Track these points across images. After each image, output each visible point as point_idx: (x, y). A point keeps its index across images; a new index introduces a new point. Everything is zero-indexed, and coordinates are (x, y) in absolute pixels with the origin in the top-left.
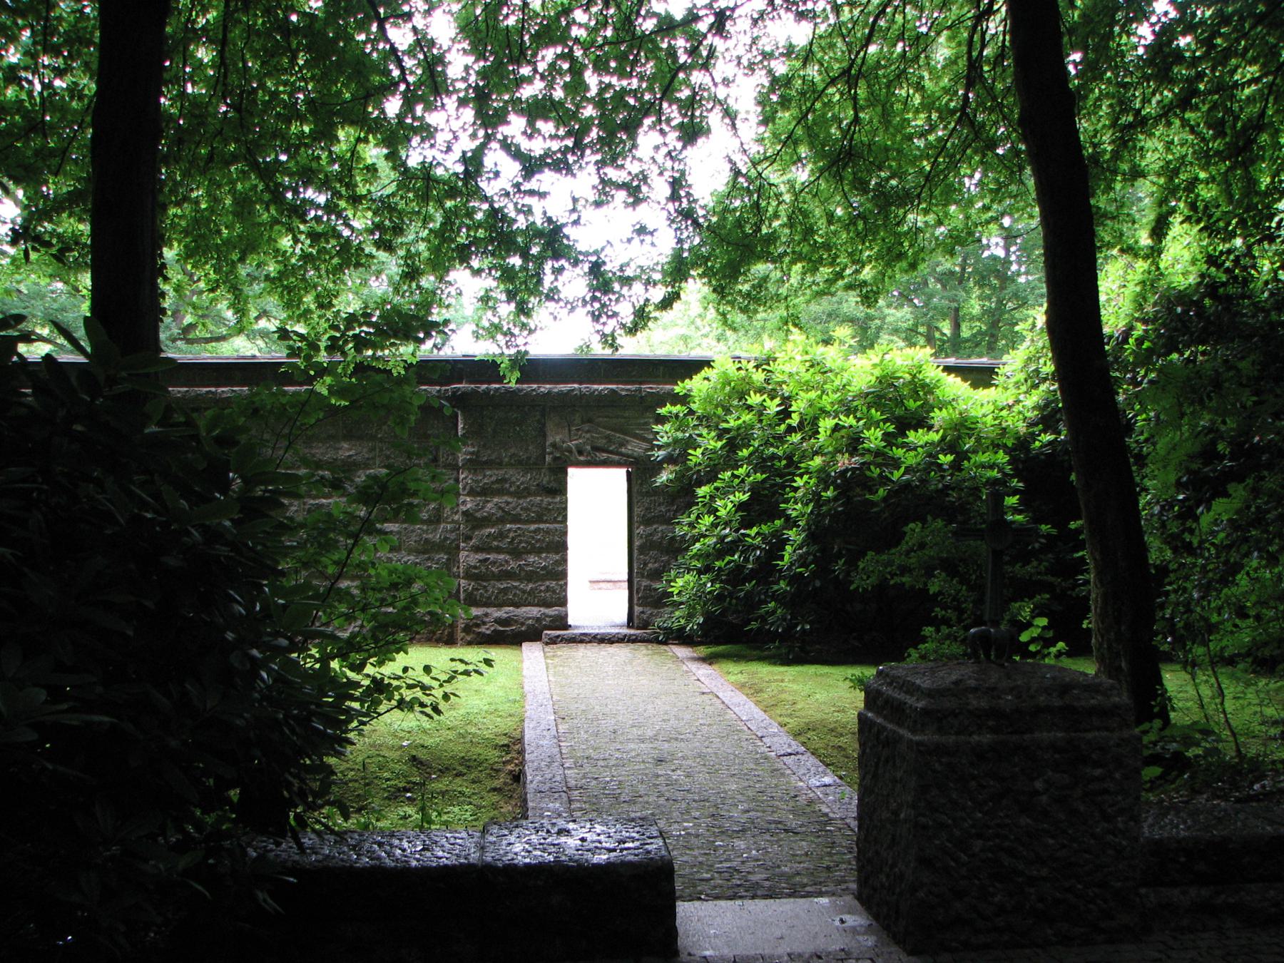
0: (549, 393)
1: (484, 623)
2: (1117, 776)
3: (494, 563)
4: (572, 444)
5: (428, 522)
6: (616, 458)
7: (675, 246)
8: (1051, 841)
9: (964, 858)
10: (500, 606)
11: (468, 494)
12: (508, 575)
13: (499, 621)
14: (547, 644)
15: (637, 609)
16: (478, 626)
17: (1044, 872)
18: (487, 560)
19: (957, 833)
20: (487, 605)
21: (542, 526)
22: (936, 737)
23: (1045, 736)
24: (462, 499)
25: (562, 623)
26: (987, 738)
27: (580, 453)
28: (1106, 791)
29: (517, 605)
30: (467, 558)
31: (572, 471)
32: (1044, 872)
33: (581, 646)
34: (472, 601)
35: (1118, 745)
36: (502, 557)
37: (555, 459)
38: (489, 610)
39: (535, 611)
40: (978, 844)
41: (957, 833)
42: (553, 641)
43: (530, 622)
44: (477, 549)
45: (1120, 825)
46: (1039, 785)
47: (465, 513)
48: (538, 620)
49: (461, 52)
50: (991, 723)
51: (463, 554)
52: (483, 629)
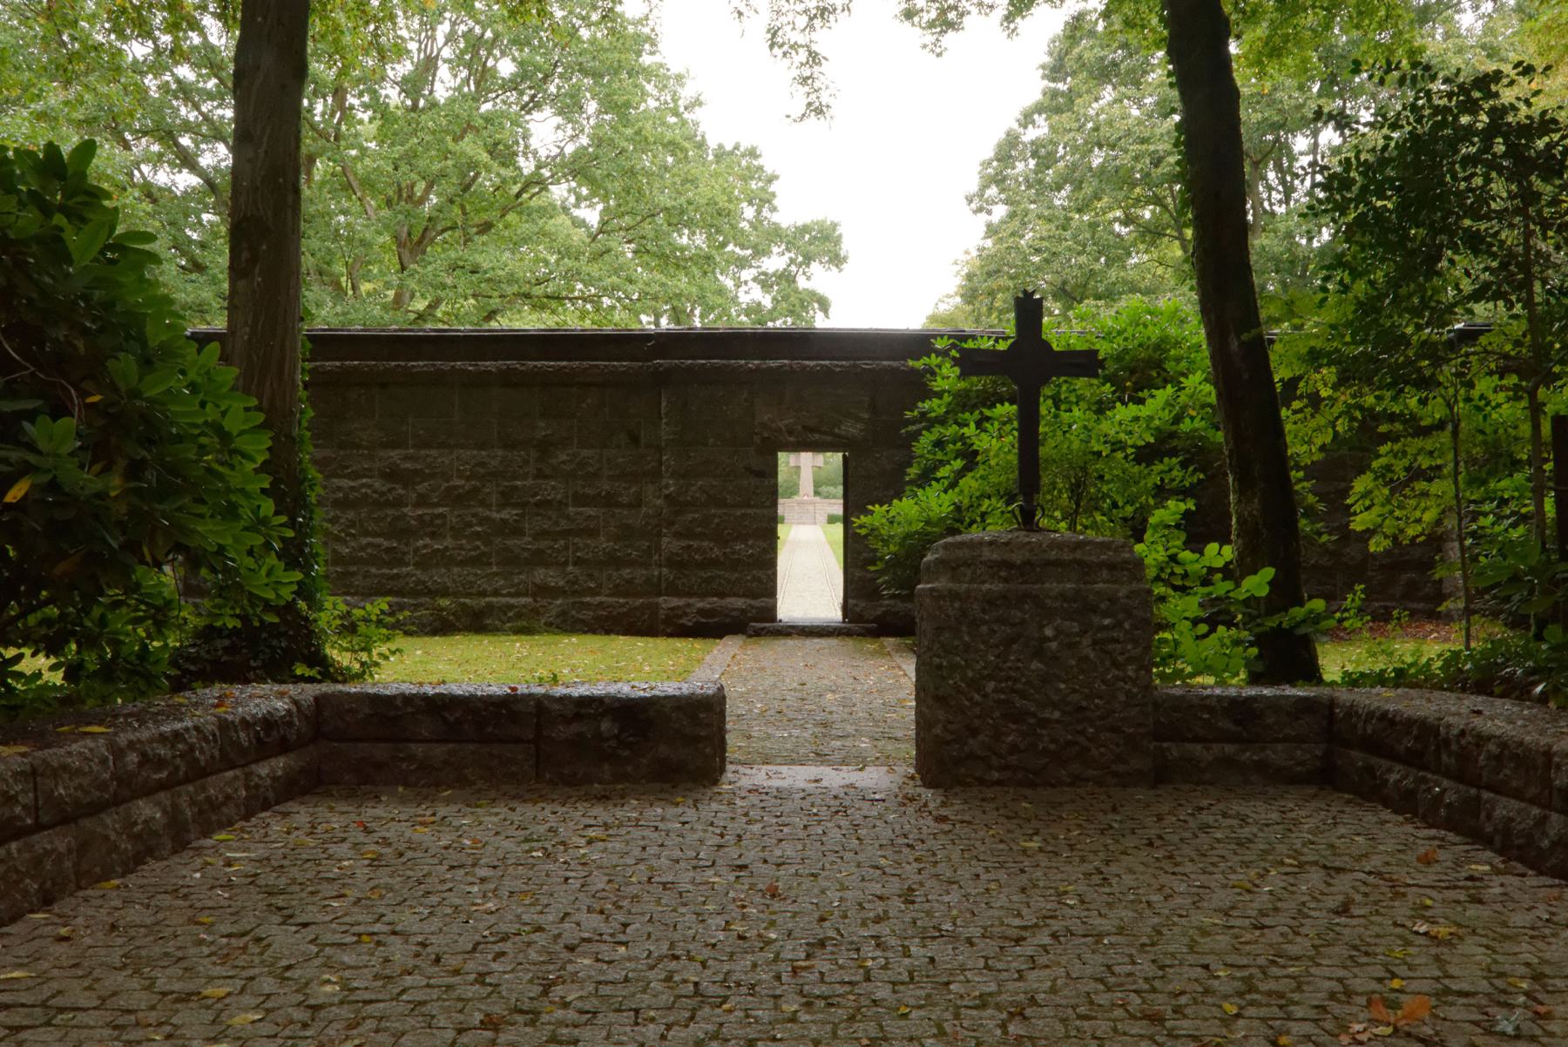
0: (758, 368)
1: (686, 614)
2: (1127, 626)
3: (698, 550)
4: (781, 424)
5: (630, 506)
6: (829, 438)
7: (981, 243)
8: (1063, 686)
9: (977, 697)
10: (703, 596)
11: (672, 476)
12: (714, 563)
13: (701, 612)
14: (750, 636)
15: (851, 601)
16: (680, 617)
17: (1057, 715)
18: (690, 547)
19: (970, 674)
20: (690, 594)
21: (750, 511)
22: (950, 585)
23: (1053, 587)
24: (664, 481)
25: (770, 613)
26: (996, 587)
27: (790, 433)
28: (1117, 641)
29: (722, 595)
30: (670, 544)
31: (780, 454)
32: (1057, 715)
33: (790, 642)
34: (673, 591)
35: (1127, 597)
36: (705, 544)
37: (764, 439)
38: (691, 601)
39: (740, 603)
40: (991, 685)
41: (970, 674)
42: (758, 634)
43: (735, 613)
44: (678, 535)
45: (1130, 673)
46: (1049, 632)
47: (667, 497)
48: (743, 611)
49: (817, 22)
50: (1003, 574)
51: (665, 540)
52: (684, 621)
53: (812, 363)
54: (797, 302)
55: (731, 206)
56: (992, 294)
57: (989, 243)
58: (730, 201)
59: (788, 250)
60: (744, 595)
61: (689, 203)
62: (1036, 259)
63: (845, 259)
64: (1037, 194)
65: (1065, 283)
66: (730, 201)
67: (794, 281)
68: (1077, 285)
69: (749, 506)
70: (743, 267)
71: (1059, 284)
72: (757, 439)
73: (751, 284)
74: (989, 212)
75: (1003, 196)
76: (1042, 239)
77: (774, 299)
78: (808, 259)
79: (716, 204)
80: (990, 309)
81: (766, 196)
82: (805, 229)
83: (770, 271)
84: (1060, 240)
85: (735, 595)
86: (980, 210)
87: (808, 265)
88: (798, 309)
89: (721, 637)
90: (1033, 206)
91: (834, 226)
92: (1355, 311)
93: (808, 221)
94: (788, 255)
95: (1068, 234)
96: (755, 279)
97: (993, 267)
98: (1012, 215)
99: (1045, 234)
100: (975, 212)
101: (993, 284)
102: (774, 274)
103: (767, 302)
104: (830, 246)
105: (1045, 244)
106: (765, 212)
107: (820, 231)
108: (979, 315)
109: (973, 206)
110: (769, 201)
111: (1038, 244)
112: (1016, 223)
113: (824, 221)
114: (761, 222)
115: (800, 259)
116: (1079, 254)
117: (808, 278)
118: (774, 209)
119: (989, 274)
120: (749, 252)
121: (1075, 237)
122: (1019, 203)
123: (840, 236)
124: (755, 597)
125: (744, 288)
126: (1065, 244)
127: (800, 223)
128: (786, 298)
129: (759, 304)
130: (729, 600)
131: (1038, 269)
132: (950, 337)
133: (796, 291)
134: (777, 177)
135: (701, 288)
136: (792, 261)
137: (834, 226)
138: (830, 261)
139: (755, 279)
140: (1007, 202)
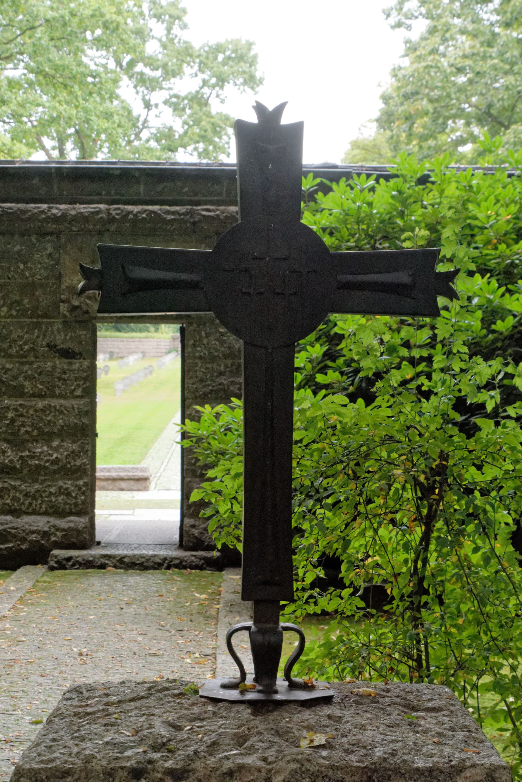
29: (16, 513)
43: (33, 537)
48: (45, 534)
53: (136, 209)
54: (209, 127)
55: (120, 19)
56: (409, 118)
57: (406, 62)
58: (119, 13)
59: (201, 70)
60: (46, 513)
61: (73, 14)
62: (462, 79)
63: (261, 81)
64: (462, 7)
65: (490, 106)
66: (119, 13)
67: (206, 104)
68: (504, 109)
69: (53, 396)
70: (153, 89)
71: (483, 107)
72: (64, 308)
73: (162, 107)
74: (409, 28)
75: (423, 10)
76: (465, 57)
77: (185, 123)
78: (222, 81)
79: (102, 15)
80: (410, 136)
81: (174, 12)
82: (219, 49)
83: (183, 94)
84: (484, 58)
85: (35, 513)
86: (399, 25)
87: (222, 87)
88: (210, 134)
89: (14, 568)
90: (457, 21)
91: (250, 45)
92: (508, 222)
93: (222, 40)
94: (201, 76)
95: (494, 51)
96: (165, 102)
97: (409, 89)
98: (432, 31)
99: (468, 51)
100: (393, 27)
101: (408, 107)
102: (186, 98)
103: (179, 128)
104: (244, 67)
105: (468, 62)
106: (176, 30)
107: (235, 51)
108: (398, 142)
109: (393, 19)
110: (179, 18)
111: (460, 63)
112: (437, 39)
113: (239, 40)
114: (172, 41)
115: (214, 80)
116: (506, 73)
117: (223, 101)
118: (184, 26)
119: (406, 97)
120: (158, 73)
121: (501, 54)
122: (440, 16)
123: (255, 57)
124: (61, 514)
125: (154, 111)
126: (490, 62)
127: (213, 42)
128: (197, 122)
129: (170, 129)
130: (26, 519)
131: (461, 90)
132: (316, 175)
133: (208, 115)
134: (387, 19)
135: (86, 111)
136: (205, 83)
137: (250, 45)
138: (245, 83)
139: (165, 102)
140: (429, 16)
